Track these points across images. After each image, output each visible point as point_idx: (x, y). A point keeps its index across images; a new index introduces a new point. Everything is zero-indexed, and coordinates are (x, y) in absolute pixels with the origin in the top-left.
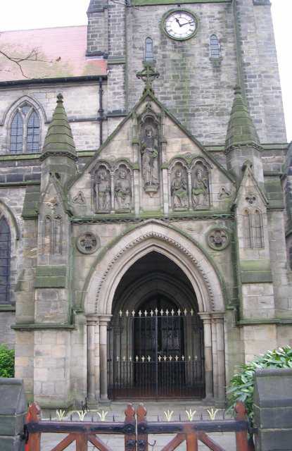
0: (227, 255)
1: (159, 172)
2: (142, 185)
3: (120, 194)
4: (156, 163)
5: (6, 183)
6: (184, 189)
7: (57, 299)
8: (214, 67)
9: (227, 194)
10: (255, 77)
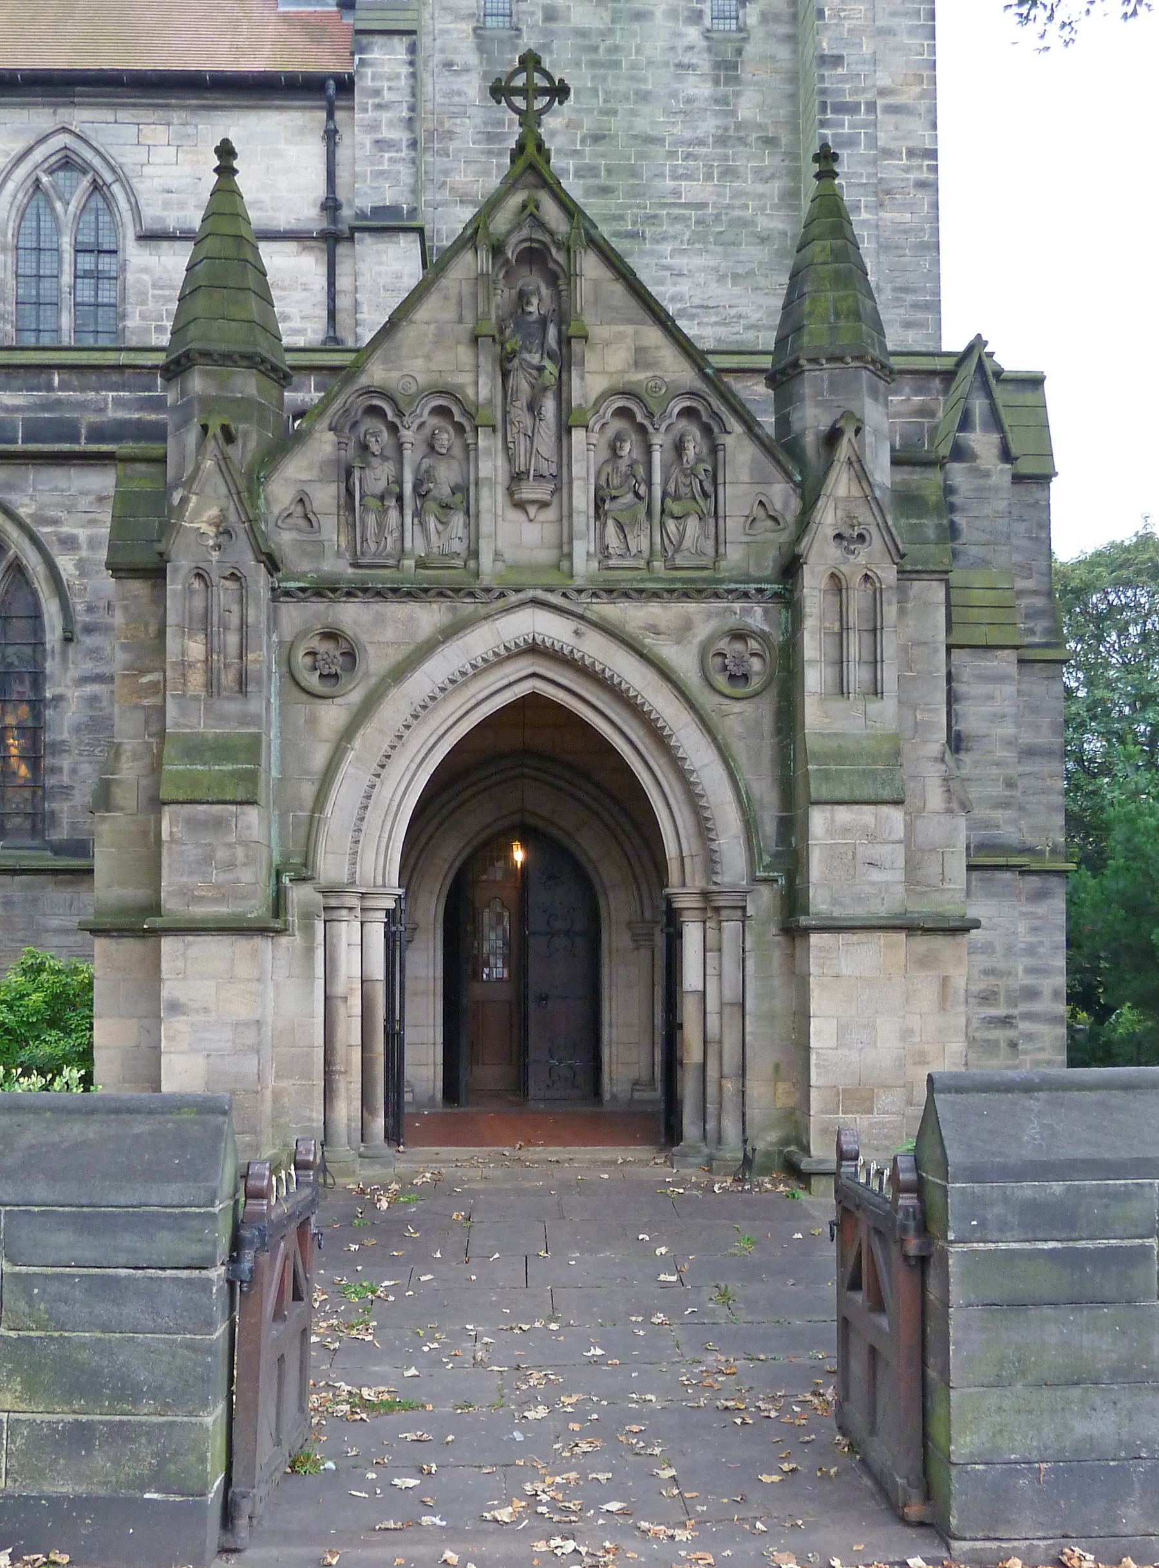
0: (763, 711)
1: (560, 439)
2: (502, 478)
3: (431, 506)
4: (549, 406)
5: (19, 446)
7: (232, 839)
8: (717, 65)
9: (774, 519)
10: (853, 109)
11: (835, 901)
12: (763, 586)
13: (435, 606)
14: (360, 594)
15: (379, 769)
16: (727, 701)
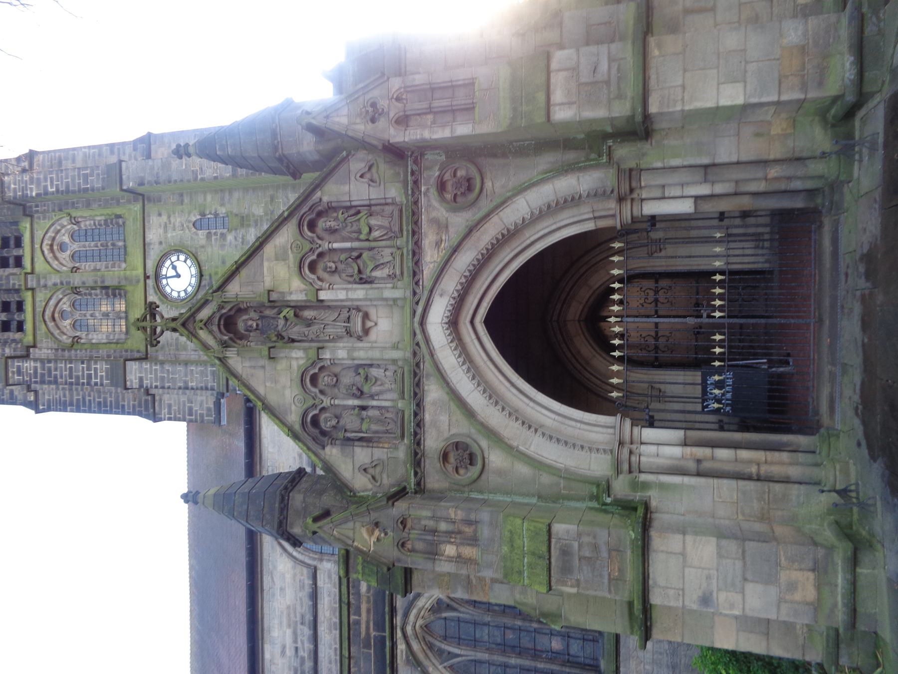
4: (308, 314)
6: (359, 256)
8: (242, 225)
9: (370, 168)
11: (620, 96)
12: (410, 170)
13: (426, 388)
14: (418, 437)
15: (533, 429)
16: (485, 191)
